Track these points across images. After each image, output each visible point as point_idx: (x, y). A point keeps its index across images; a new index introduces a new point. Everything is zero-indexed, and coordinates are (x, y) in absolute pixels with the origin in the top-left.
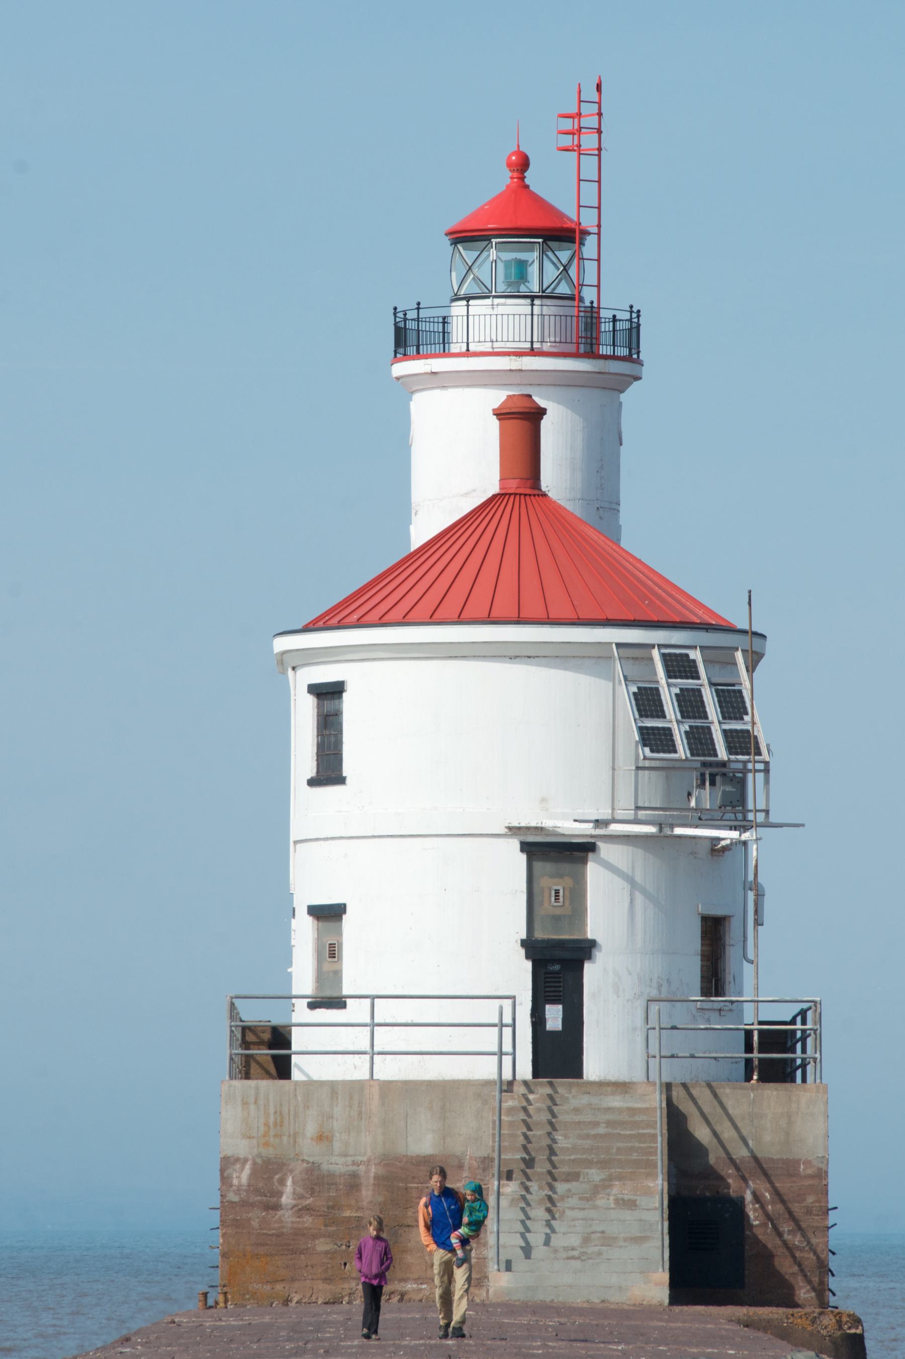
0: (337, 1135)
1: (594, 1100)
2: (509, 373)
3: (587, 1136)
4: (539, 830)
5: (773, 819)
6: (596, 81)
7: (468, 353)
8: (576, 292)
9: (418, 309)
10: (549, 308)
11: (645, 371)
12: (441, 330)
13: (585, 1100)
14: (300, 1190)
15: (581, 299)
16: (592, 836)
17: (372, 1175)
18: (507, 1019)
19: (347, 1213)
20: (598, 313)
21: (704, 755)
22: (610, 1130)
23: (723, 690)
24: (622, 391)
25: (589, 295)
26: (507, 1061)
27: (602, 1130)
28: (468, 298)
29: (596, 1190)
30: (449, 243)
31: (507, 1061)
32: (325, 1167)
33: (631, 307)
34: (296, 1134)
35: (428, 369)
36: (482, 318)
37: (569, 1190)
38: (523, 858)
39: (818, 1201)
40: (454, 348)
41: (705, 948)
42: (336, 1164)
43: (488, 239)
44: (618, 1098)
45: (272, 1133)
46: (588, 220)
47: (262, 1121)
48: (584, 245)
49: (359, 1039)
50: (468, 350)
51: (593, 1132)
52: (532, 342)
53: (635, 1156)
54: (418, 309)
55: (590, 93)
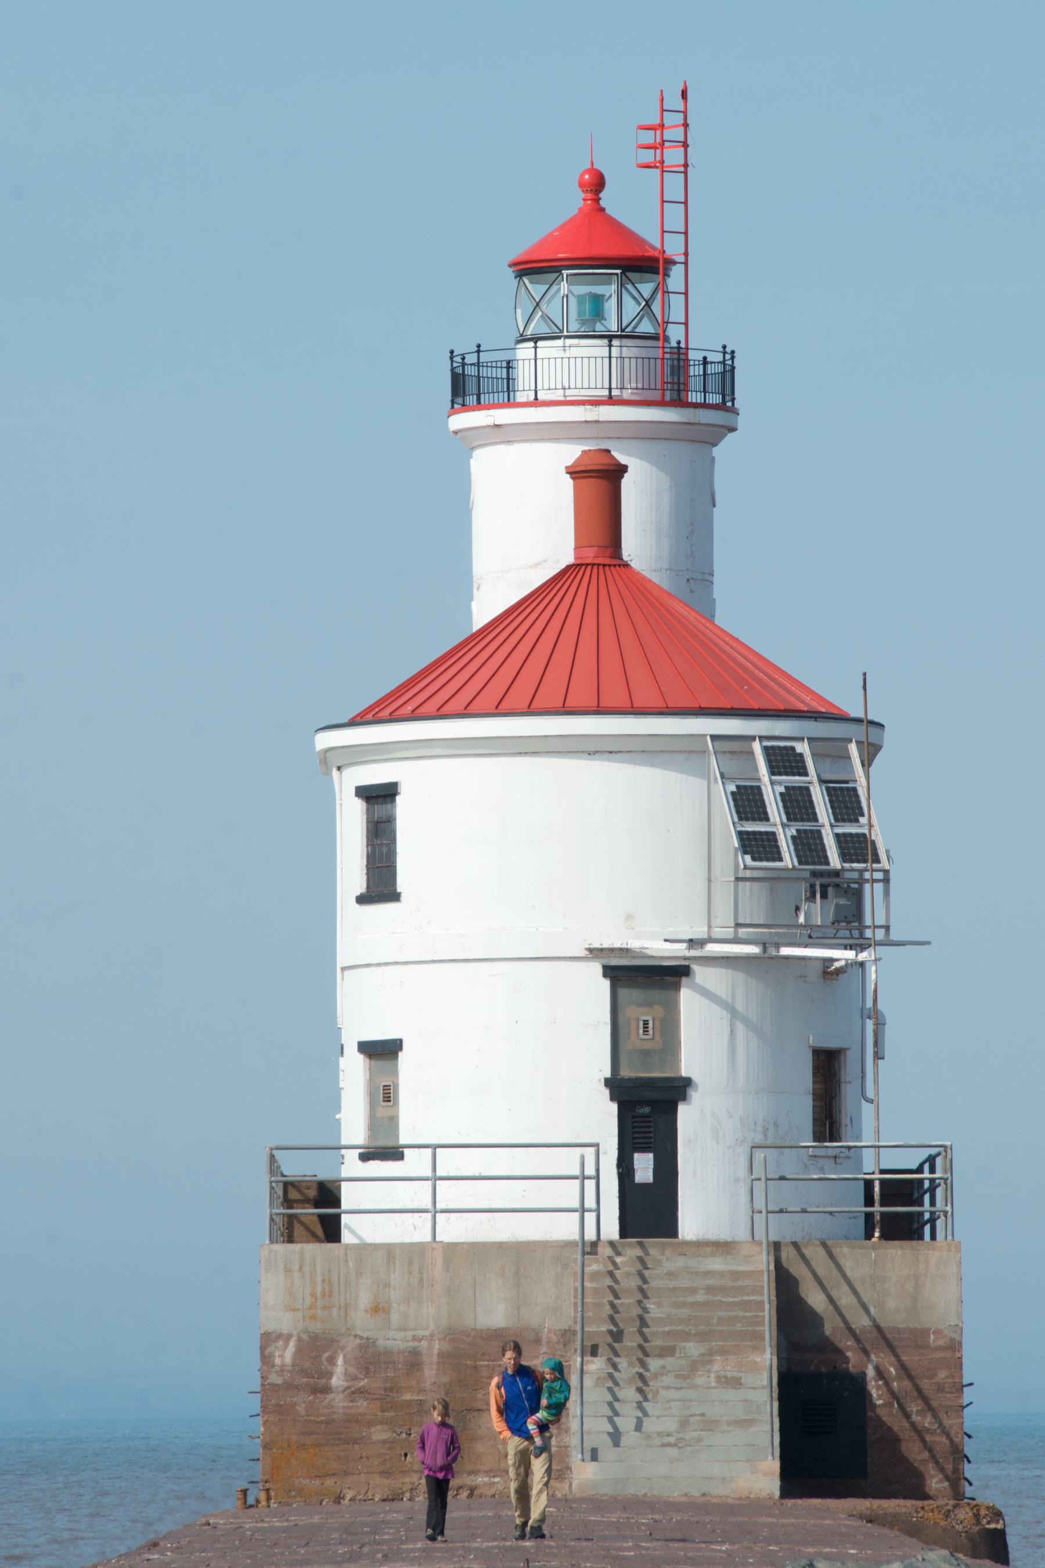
0: (395, 1305)
1: (692, 1263)
2: (584, 425)
3: (684, 1305)
4: (625, 951)
5: (894, 936)
6: (681, 87)
7: (536, 403)
8: (660, 331)
9: (478, 352)
10: (630, 350)
11: (741, 421)
12: (505, 376)
13: (680, 1262)
14: (352, 1370)
15: (666, 339)
16: (685, 958)
17: (436, 1351)
18: (590, 1171)
19: (408, 1396)
20: (686, 354)
21: (814, 863)
22: (710, 1298)
23: (835, 788)
24: (715, 445)
25: (675, 334)
26: (590, 1218)
27: (700, 1297)
28: (535, 339)
29: (695, 1366)
30: (513, 275)
31: (590, 1218)
32: (381, 1343)
33: (724, 347)
35: (490, 421)
36: (552, 361)
37: (664, 1367)
38: (606, 984)
39: (951, 1376)
40: (521, 397)
42: (394, 1340)
43: (558, 270)
44: (719, 1260)
45: (319, 1304)
46: (673, 247)
47: (308, 1290)
48: (669, 276)
49: (419, 1195)
50: (536, 399)
51: (690, 1300)
52: (610, 389)
53: (739, 1327)
54: (478, 352)
55: (674, 101)
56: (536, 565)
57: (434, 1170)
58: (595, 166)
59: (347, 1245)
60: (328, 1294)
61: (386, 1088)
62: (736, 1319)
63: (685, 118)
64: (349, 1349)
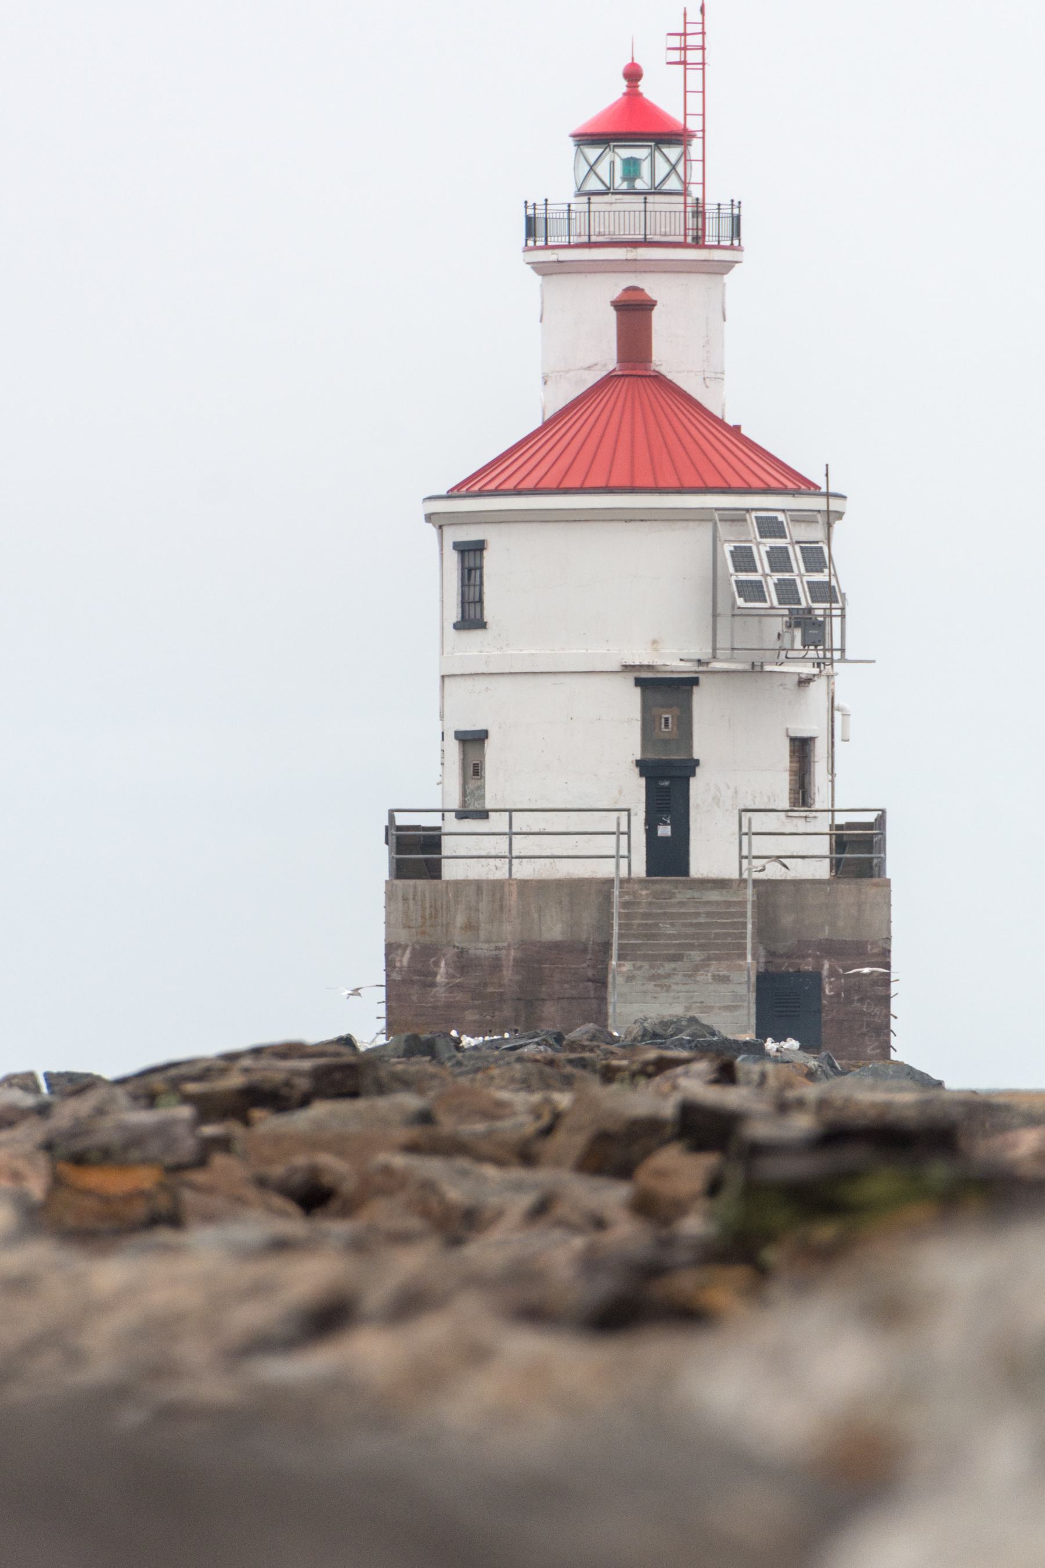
1: (696, 895)
3: (691, 925)
4: (650, 668)
5: (848, 656)
6: (700, 5)
11: (745, 256)
13: (689, 894)
14: (451, 971)
16: (696, 672)
18: (624, 828)
19: (490, 990)
20: (703, 207)
21: (790, 604)
22: (708, 920)
25: (696, 191)
26: (624, 863)
27: (702, 920)
29: (697, 968)
31: (624, 863)
32: (472, 951)
34: (448, 924)
37: (675, 969)
38: (638, 691)
41: (794, 765)
42: (482, 949)
44: (716, 892)
45: (428, 923)
46: (694, 124)
47: (420, 913)
49: (501, 845)
51: (694, 921)
53: (729, 940)
55: (694, 16)
56: (589, 368)
58: (636, 61)
59: (448, 881)
60: (434, 916)
61: (475, 765)
62: (727, 935)
63: (703, 28)
64: (448, 956)
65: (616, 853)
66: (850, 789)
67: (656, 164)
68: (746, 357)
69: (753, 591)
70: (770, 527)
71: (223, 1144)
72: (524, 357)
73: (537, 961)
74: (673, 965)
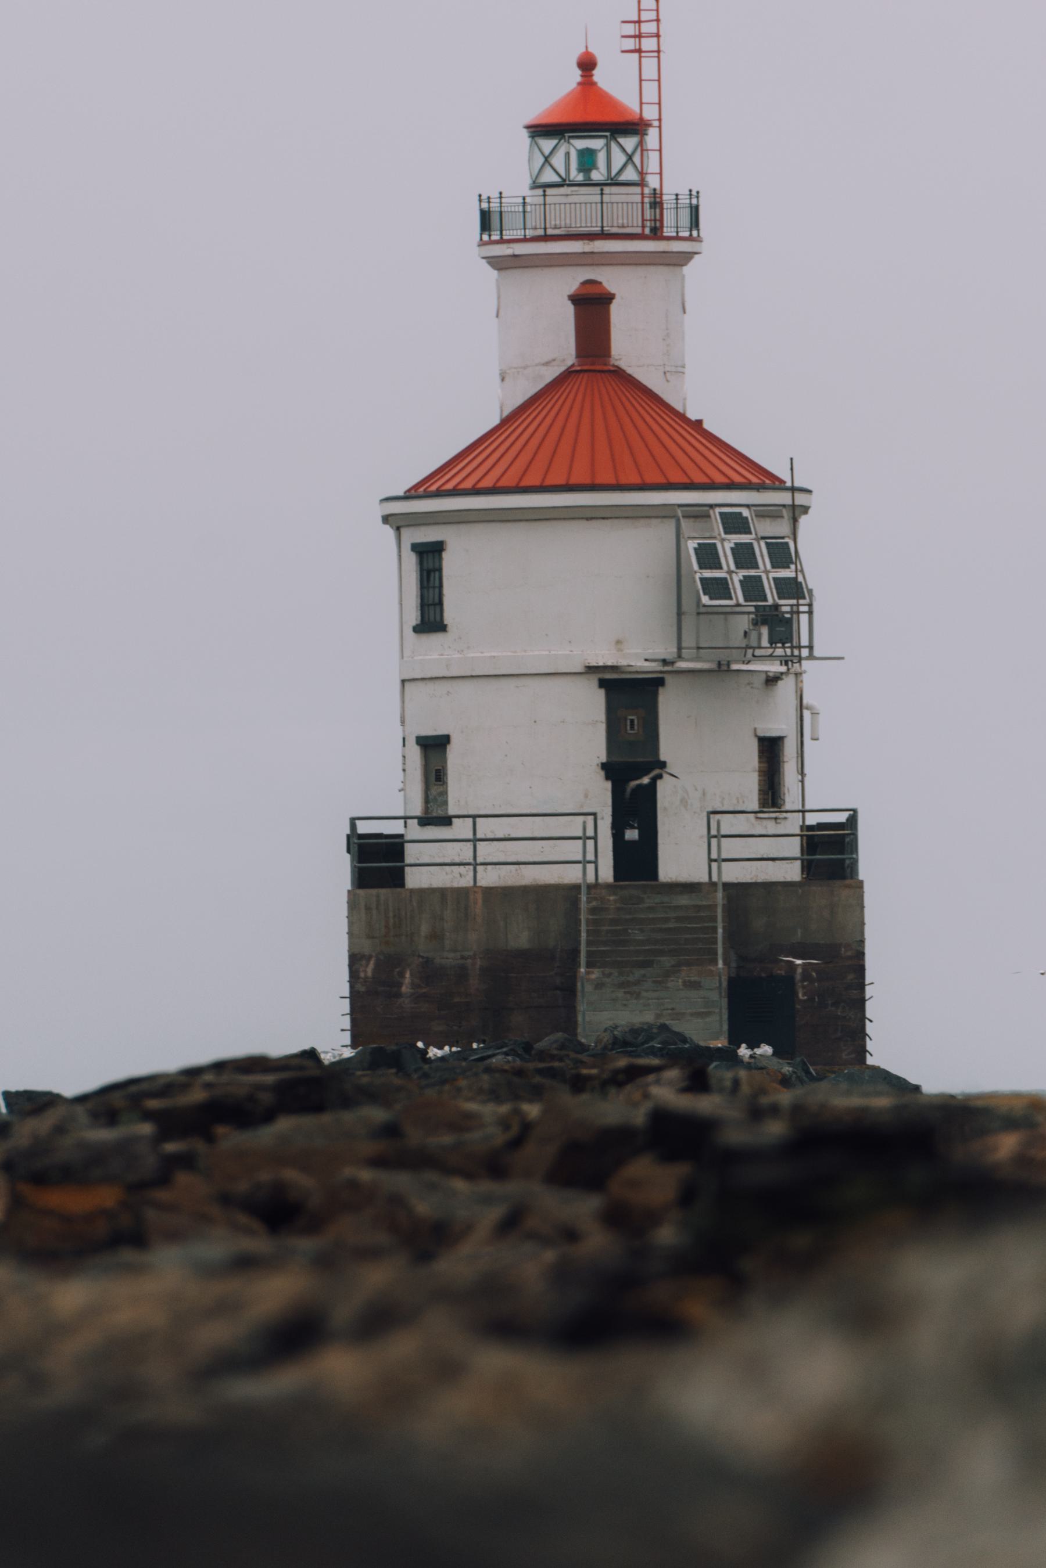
1: (666, 899)
4: (614, 668)
11: (704, 247)
16: (661, 672)
17: (478, 967)
18: (590, 832)
19: (457, 1000)
20: (661, 198)
25: (653, 182)
26: (590, 868)
27: (671, 925)
31: (590, 868)
37: (644, 976)
42: (448, 959)
49: (465, 852)
56: (547, 364)
57: (469, 864)
58: (590, 50)
61: (438, 771)
63: (658, 15)
65: (573, 854)
66: (821, 788)
67: (612, 156)
68: (712, 352)
69: (718, 588)
70: (735, 523)
71: (186, 1161)
72: (477, 355)
73: (504, 969)
74: (642, 972)
